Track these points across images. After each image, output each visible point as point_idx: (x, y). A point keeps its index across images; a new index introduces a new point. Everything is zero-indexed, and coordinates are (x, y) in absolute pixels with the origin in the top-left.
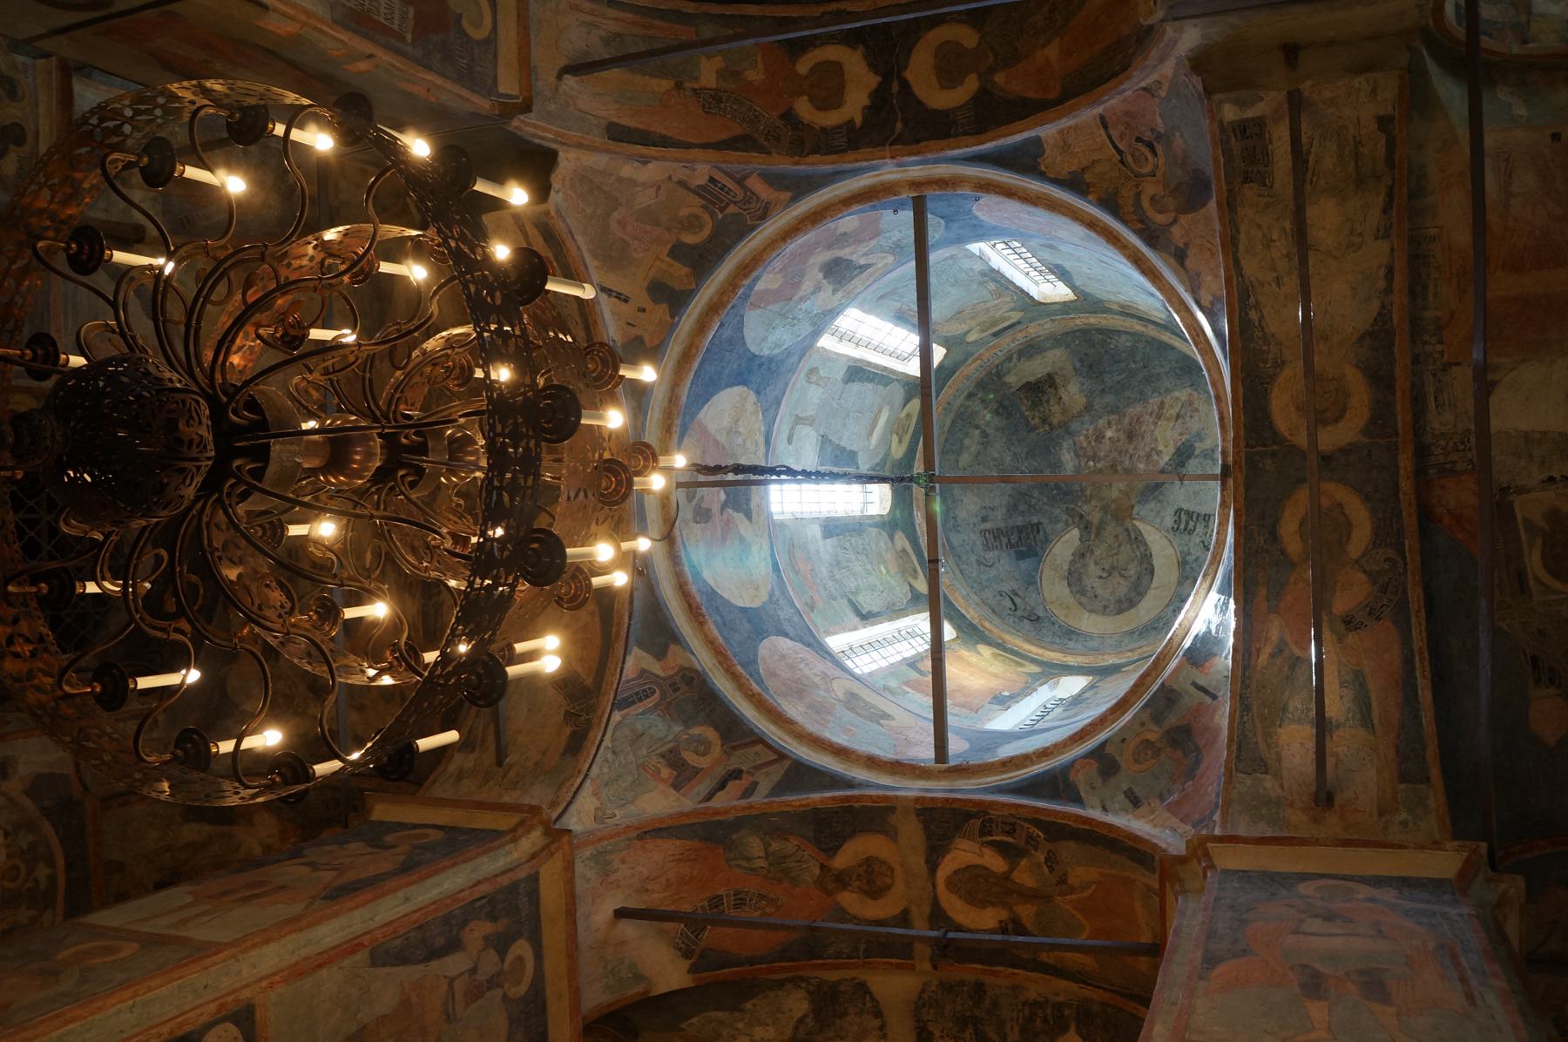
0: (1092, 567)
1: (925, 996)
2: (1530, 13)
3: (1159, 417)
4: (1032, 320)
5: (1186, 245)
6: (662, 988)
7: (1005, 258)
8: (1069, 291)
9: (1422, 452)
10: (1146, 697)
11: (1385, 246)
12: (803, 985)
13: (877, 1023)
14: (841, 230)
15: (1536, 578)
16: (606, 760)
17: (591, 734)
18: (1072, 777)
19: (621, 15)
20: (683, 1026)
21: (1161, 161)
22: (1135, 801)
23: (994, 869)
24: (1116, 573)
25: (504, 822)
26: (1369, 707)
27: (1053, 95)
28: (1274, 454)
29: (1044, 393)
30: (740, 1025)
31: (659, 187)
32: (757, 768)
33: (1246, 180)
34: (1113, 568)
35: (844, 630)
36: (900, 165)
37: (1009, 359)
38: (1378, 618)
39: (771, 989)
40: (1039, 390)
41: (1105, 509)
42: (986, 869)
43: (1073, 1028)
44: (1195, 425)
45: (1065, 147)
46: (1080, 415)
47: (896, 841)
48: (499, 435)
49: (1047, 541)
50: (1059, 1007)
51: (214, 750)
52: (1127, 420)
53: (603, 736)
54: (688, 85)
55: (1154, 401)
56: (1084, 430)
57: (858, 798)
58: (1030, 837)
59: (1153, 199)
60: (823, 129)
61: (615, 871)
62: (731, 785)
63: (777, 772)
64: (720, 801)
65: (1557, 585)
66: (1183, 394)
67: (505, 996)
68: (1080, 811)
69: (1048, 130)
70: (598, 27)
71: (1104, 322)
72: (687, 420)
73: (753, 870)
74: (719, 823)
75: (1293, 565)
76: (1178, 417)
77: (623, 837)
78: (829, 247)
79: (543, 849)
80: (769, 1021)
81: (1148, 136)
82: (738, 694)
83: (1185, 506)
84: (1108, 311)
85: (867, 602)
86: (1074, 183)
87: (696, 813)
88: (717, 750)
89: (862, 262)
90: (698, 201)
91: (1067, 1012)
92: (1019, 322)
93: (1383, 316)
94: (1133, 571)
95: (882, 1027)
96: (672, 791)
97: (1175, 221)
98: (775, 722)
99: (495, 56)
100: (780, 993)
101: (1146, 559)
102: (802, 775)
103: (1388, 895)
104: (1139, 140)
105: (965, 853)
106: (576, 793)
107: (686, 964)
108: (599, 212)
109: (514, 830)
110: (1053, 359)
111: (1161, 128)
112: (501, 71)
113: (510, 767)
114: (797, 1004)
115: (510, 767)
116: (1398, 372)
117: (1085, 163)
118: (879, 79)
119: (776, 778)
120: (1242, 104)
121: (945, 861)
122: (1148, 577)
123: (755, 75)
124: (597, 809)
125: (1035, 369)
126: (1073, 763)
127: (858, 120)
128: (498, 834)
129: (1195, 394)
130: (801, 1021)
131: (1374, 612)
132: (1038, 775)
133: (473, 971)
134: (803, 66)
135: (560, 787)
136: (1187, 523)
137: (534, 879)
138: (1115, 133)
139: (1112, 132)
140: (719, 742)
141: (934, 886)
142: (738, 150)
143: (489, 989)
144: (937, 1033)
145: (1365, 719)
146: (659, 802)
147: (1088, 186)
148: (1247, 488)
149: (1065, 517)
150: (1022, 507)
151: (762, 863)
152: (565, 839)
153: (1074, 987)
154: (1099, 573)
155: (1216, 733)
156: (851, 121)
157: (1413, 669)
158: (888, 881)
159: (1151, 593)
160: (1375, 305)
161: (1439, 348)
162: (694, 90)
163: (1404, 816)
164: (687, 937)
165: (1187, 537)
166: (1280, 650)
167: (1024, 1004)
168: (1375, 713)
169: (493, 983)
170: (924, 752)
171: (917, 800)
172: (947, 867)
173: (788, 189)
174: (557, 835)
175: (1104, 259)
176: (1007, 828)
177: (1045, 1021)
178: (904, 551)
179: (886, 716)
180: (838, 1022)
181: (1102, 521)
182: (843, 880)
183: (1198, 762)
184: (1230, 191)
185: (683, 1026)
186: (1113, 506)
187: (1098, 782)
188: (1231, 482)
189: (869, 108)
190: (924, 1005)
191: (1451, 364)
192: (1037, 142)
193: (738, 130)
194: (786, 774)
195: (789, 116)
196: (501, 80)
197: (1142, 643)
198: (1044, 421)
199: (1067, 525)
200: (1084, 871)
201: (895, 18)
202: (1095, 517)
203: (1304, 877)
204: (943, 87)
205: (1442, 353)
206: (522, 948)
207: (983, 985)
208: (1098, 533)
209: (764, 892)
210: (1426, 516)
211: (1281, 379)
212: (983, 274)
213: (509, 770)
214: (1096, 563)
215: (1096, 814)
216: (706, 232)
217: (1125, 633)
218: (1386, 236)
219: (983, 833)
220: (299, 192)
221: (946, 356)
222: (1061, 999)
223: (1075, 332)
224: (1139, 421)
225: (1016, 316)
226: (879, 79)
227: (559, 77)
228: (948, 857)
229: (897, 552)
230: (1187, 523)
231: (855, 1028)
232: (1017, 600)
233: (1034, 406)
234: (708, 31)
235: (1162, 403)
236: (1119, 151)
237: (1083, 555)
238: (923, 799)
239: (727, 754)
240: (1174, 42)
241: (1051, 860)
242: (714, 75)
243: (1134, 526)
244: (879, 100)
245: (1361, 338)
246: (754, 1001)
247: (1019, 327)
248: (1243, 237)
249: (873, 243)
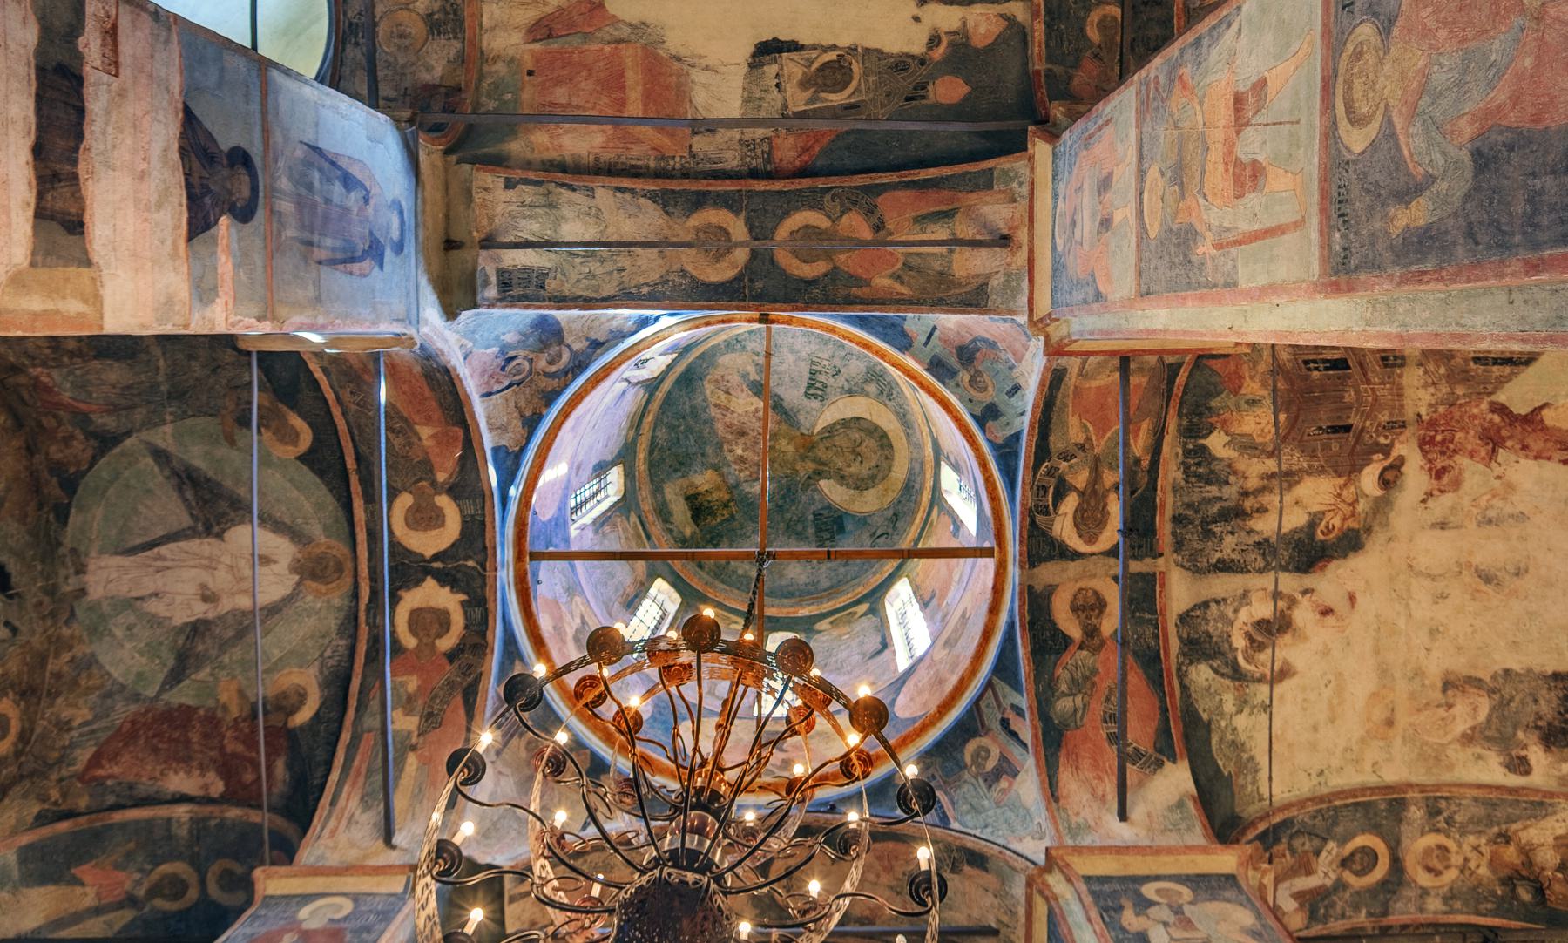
0: (852, 469)
1: (1188, 565)
2: (440, 86)
3: (727, 409)
4: (638, 505)
5: (587, 339)
6: (1190, 786)
7: (584, 515)
8: (615, 469)
9: (754, 174)
10: (937, 384)
11: (599, 192)
12: (1184, 668)
13: (1213, 606)
14: (551, 629)
15: (849, 97)
16: (992, 833)
17: (969, 845)
18: (1000, 441)
19: (344, 795)
20: (1226, 773)
21: (522, 353)
22: (1016, 389)
23: (1076, 504)
24: (858, 449)
25: (1041, 909)
26: (940, 213)
27: (461, 433)
28: (751, 280)
29: (701, 505)
30: (1223, 724)
31: (500, 773)
32: (999, 705)
33: (543, 287)
34: (853, 451)
35: (894, 660)
36: (503, 566)
37: (670, 531)
38: (876, 206)
39: (1190, 696)
40: (698, 508)
41: (803, 458)
42: (1076, 511)
43: (1202, 441)
44: (735, 379)
45: (503, 429)
46: (721, 475)
47: (1057, 586)
48: (888, 836)
49: (829, 507)
50: (1187, 453)
51: (751, 825)
52: (729, 436)
53: (322, 831)
54: (414, 740)
55: (713, 412)
56: (735, 473)
57: (1022, 617)
58: (1049, 473)
59: (550, 363)
60: (466, 627)
61: (1085, 820)
62: (1013, 727)
63: (1003, 688)
64: (1027, 735)
65: (854, 84)
66: (708, 387)
67: (1191, 903)
68: (1025, 433)
69: (488, 441)
70: (353, 815)
71: (644, 446)
72: (413, 14)
73: (1085, 706)
74: (1044, 734)
75: (835, 268)
76: (727, 393)
77: (1056, 814)
78: (564, 642)
79: (1063, 872)
80: (1218, 698)
81: (500, 361)
82: (939, 725)
83: (803, 390)
84: (634, 441)
85: (873, 642)
86: (532, 423)
87: (1036, 753)
88: (984, 741)
89: (578, 621)
90: (515, 740)
91: (1190, 446)
92: (639, 517)
93: (653, 197)
94: (856, 435)
95: (1217, 602)
96: (1019, 778)
97: (568, 346)
98: (962, 693)
99: (369, 895)
100: (1192, 688)
101: (846, 424)
102: (1005, 668)
103: (1062, 187)
104: (503, 369)
105: (1064, 527)
106: (1018, 854)
107: (1168, 765)
108: (515, 826)
109: (1047, 899)
110: (673, 493)
111: (496, 350)
112: (384, 890)
113: (999, 921)
114: (1201, 674)
115: (999, 921)
116: (693, 188)
117: (516, 414)
118: (429, 578)
119: (1007, 689)
120: (486, 283)
121: (1071, 544)
122: (862, 422)
123: (413, 684)
124: (1033, 838)
125: (680, 510)
126: (989, 441)
127: (463, 597)
128: (1051, 914)
129: (709, 377)
130: (1216, 671)
131: (871, 210)
132: (1000, 470)
133: (1166, 924)
134: (410, 642)
135: (1013, 869)
136: (817, 388)
137: (1088, 879)
138: (496, 387)
139: (495, 390)
140: (978, 739)
141: (1092, 554)
142: (475, 700)
143: (1183, 913)
144: (1218, 555)
145: (948, 215)
146: (1028, 787)
147: (534, 414)
148: (775, 301)
149: (809, 492)
150: (799, 528)
151: (1079, 699)
152: (1053, 853)
153: (1167, 439)
154: (858, 463)
155: (960, 325)
156: (463, 604)
157: (913, 181)
158: (1090, 593)
159: (875, 419)
160: (642, 201)
161: (678, 159)
162: (419, 735)
163: (1015, 185)
164: (1144, 763)
165: (828, 390)
166: (898, 278)
167: (1187, 482)
168: (944, 208)
169: (1178, 911)
170: (987, 566)
171: (1022, 567)
172: (1076, 543)
173: (512, 663)
174: (1052, 862)
175: (592, 424)
176: (1042, 492)
177: (1199, 464)
178: (831, 623)
179: (963, 615)
180: (1215, 639)
181: (814, 461)
182: (1091, 632)
183: (984, 340)
184: (550, 300)
185: (1226, 773)
186: (802, 451)
187: (1003, 420)
188: (774, 314)
189: (452, 588)
190: (1195, 566)
191: (691, 152)
192: (496, 450)
193: (459, 700)
194: (1004, 680)
195: (451, 656)
196: (392, 890)
197: (916, 426)
198: (726, 506)
199: (816, 490)
200: (1072, 429)
201: (383, 458)
202: (810, 466)
203: (1054, 248)
204: (443, 525)
205: (682, 157)
206: (1149, 890)
207: (1174, 517)
208: (825, 464)
209: (1103, 699)
210: (802, 173)
211: (695, 273)
212: (596, 532)
213: (398, 412)
214: (849, 466)
215: (1027, 419)
216: (783, 232)
217: (908, 441)
218: (592, 190)
219: (1047, 513)
220: (543, 735)
221: (664, 579)
222: (1180, 451)
223: (650, 474)
224: (730, 426)
225: (634, 518)
226: (429, 578)
227: (394, 847)
228: (1068, 542)
229: (500, 300)
230: (817, 388)
231: (1220, 625)
232: (879, 533)
233: (712, 513)
234: (371, 722)
235: (715, 405)
236: (510, 385)
237: (843, 477)
238: (1020, 561)
239: (987, 731)
240: (434, 329)
241: (1066, 457)
242: (408, 718)
243: (819, 433)
244: (445, 579)
245: (667, 213)
246: (1200, 711)
247: (644, 519)
248: (585, 294)
249: (563, 608)
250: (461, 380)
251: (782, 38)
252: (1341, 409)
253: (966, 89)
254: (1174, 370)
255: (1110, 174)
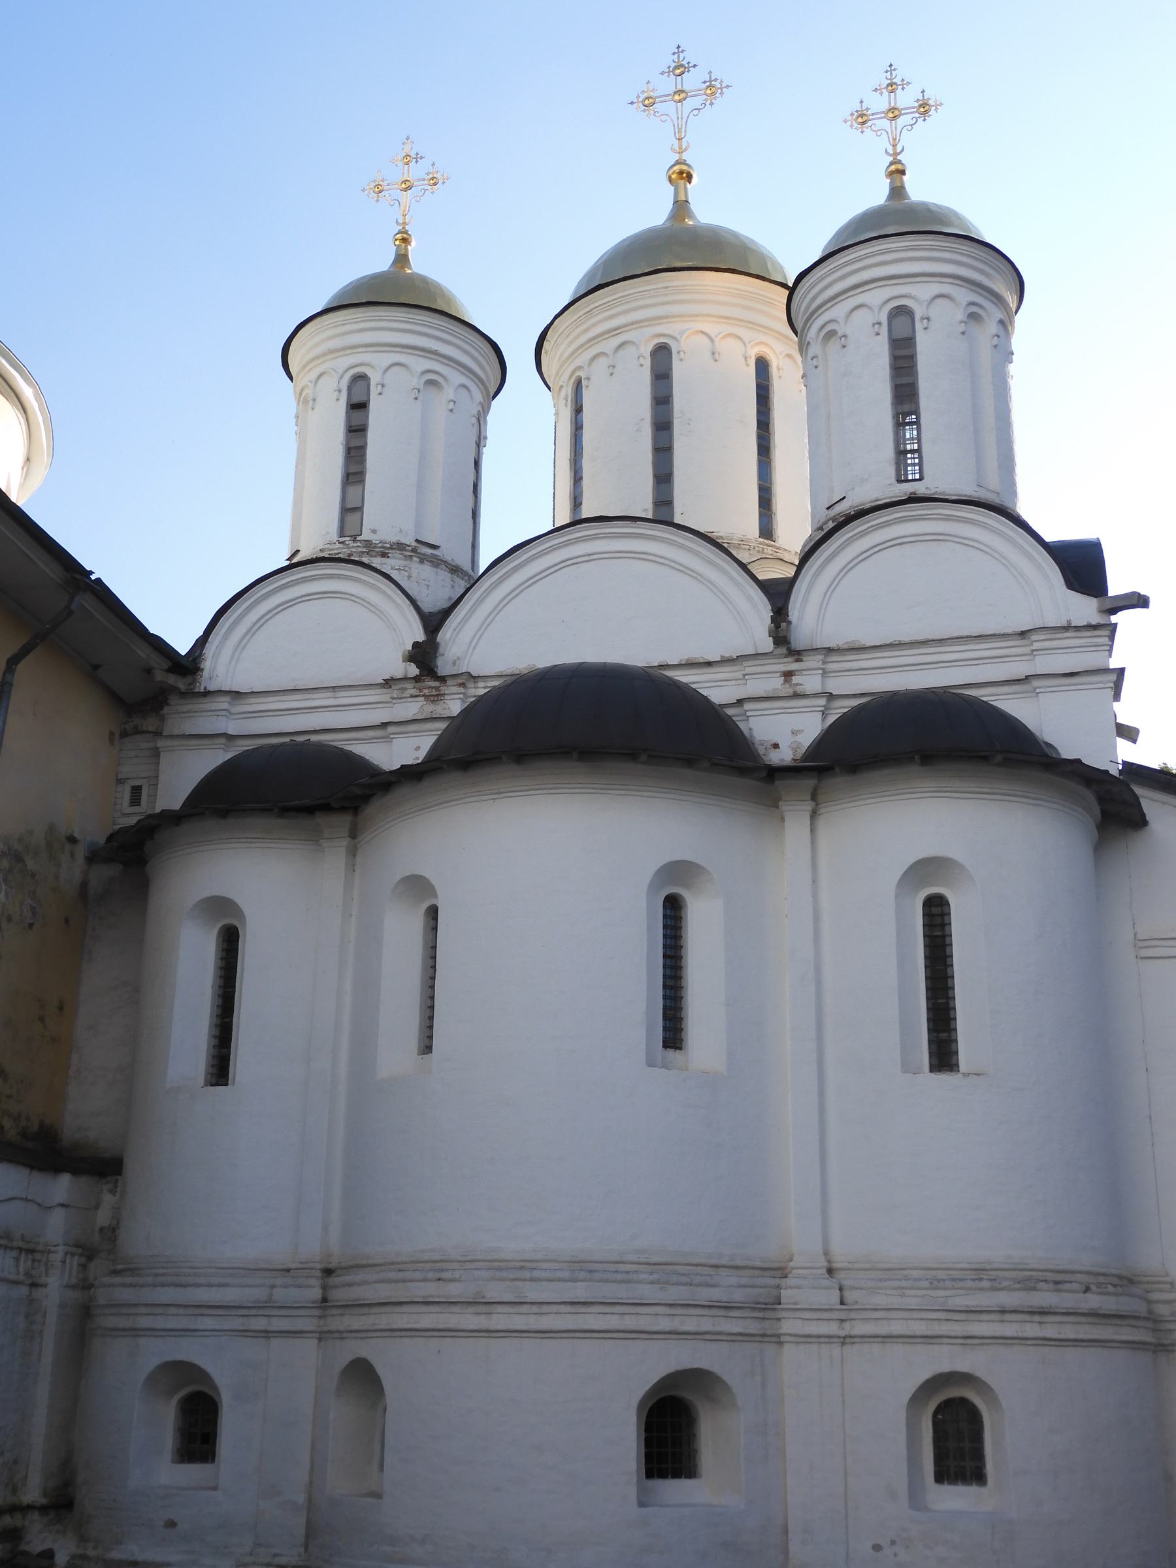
221: (159, 645)
250: (451, 292)
251: (770, 608)
252: (369, 547)
253: (791, 286)
254: (1167, 1275)
255: (292, 382)
